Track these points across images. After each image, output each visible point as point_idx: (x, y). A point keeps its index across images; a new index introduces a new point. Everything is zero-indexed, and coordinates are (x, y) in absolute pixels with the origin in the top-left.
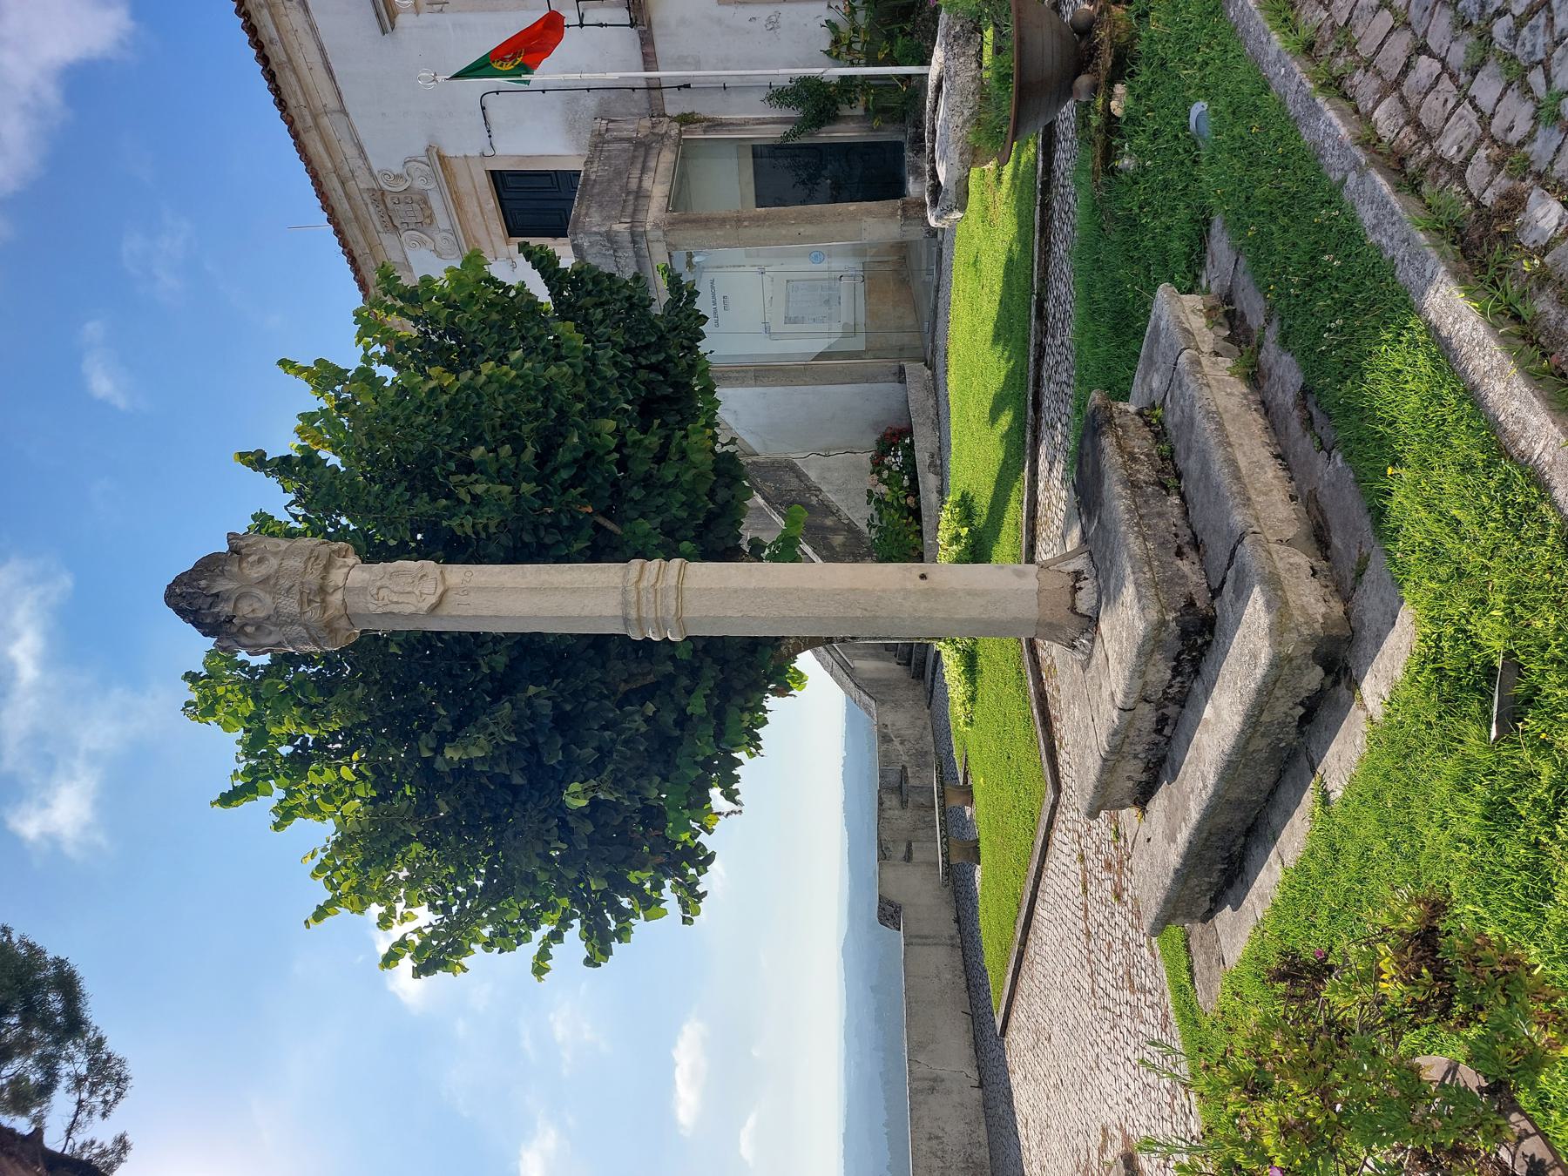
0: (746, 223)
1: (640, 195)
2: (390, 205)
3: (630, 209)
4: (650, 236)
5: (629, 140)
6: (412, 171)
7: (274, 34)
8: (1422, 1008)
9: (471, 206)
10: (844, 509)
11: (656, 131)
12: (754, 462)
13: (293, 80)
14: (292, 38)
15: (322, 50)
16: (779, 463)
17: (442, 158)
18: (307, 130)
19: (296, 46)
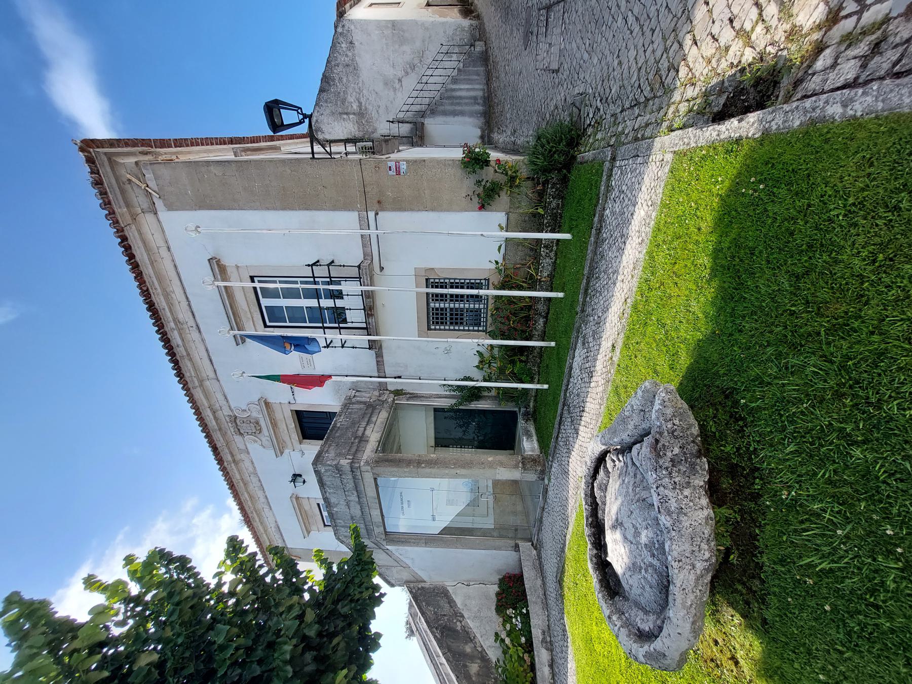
0: (423, 465)
1: (363, 439)
2: (239, 423)
3: (354, 450)
4: (363, 469)
5: (364, 403)
6: (251, 409)
7: (180, 343)
9: (282, 426)
10: (478, 636)
11: (381, 398)
12: (423, 588)
13: (189, 364)
14: (192, 344)
15: (207, 350)
16: (439, 589)
17: (267, 404)
18: (194, 388)
19: (194, 348)
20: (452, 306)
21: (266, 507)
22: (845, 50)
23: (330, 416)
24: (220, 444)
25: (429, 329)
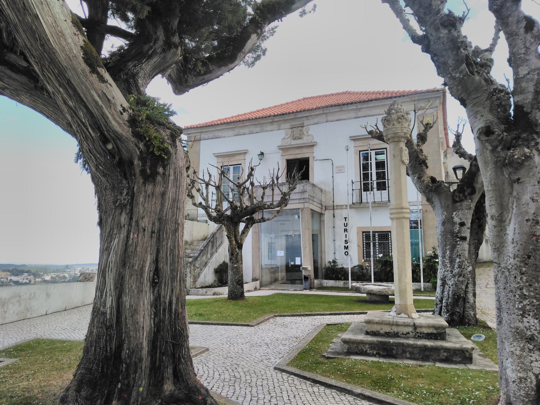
8: (499, 255)
15: (344, 119)
17: (313, 146)
18: (323, 110)
20: (377, 244)
21: (236, 133)
22: (406, 209)
23: (309, 180)
24: (286, 117)
25: (363, 232)
